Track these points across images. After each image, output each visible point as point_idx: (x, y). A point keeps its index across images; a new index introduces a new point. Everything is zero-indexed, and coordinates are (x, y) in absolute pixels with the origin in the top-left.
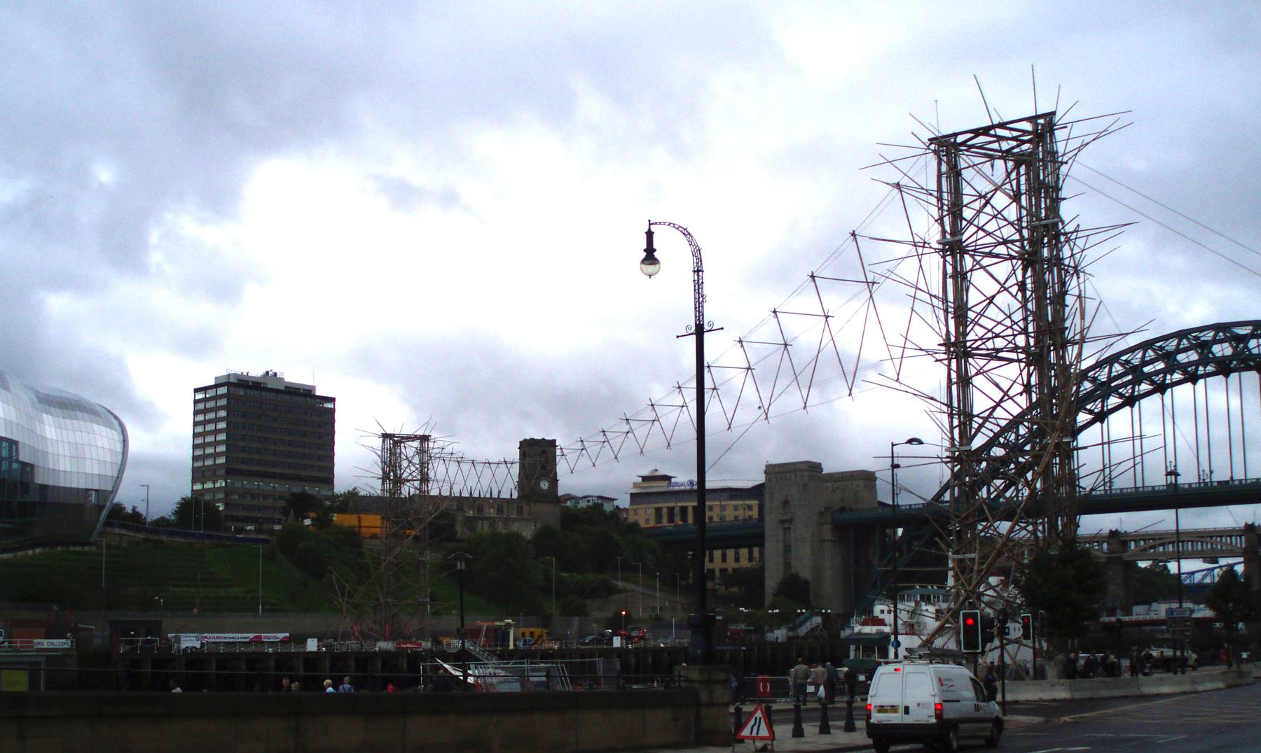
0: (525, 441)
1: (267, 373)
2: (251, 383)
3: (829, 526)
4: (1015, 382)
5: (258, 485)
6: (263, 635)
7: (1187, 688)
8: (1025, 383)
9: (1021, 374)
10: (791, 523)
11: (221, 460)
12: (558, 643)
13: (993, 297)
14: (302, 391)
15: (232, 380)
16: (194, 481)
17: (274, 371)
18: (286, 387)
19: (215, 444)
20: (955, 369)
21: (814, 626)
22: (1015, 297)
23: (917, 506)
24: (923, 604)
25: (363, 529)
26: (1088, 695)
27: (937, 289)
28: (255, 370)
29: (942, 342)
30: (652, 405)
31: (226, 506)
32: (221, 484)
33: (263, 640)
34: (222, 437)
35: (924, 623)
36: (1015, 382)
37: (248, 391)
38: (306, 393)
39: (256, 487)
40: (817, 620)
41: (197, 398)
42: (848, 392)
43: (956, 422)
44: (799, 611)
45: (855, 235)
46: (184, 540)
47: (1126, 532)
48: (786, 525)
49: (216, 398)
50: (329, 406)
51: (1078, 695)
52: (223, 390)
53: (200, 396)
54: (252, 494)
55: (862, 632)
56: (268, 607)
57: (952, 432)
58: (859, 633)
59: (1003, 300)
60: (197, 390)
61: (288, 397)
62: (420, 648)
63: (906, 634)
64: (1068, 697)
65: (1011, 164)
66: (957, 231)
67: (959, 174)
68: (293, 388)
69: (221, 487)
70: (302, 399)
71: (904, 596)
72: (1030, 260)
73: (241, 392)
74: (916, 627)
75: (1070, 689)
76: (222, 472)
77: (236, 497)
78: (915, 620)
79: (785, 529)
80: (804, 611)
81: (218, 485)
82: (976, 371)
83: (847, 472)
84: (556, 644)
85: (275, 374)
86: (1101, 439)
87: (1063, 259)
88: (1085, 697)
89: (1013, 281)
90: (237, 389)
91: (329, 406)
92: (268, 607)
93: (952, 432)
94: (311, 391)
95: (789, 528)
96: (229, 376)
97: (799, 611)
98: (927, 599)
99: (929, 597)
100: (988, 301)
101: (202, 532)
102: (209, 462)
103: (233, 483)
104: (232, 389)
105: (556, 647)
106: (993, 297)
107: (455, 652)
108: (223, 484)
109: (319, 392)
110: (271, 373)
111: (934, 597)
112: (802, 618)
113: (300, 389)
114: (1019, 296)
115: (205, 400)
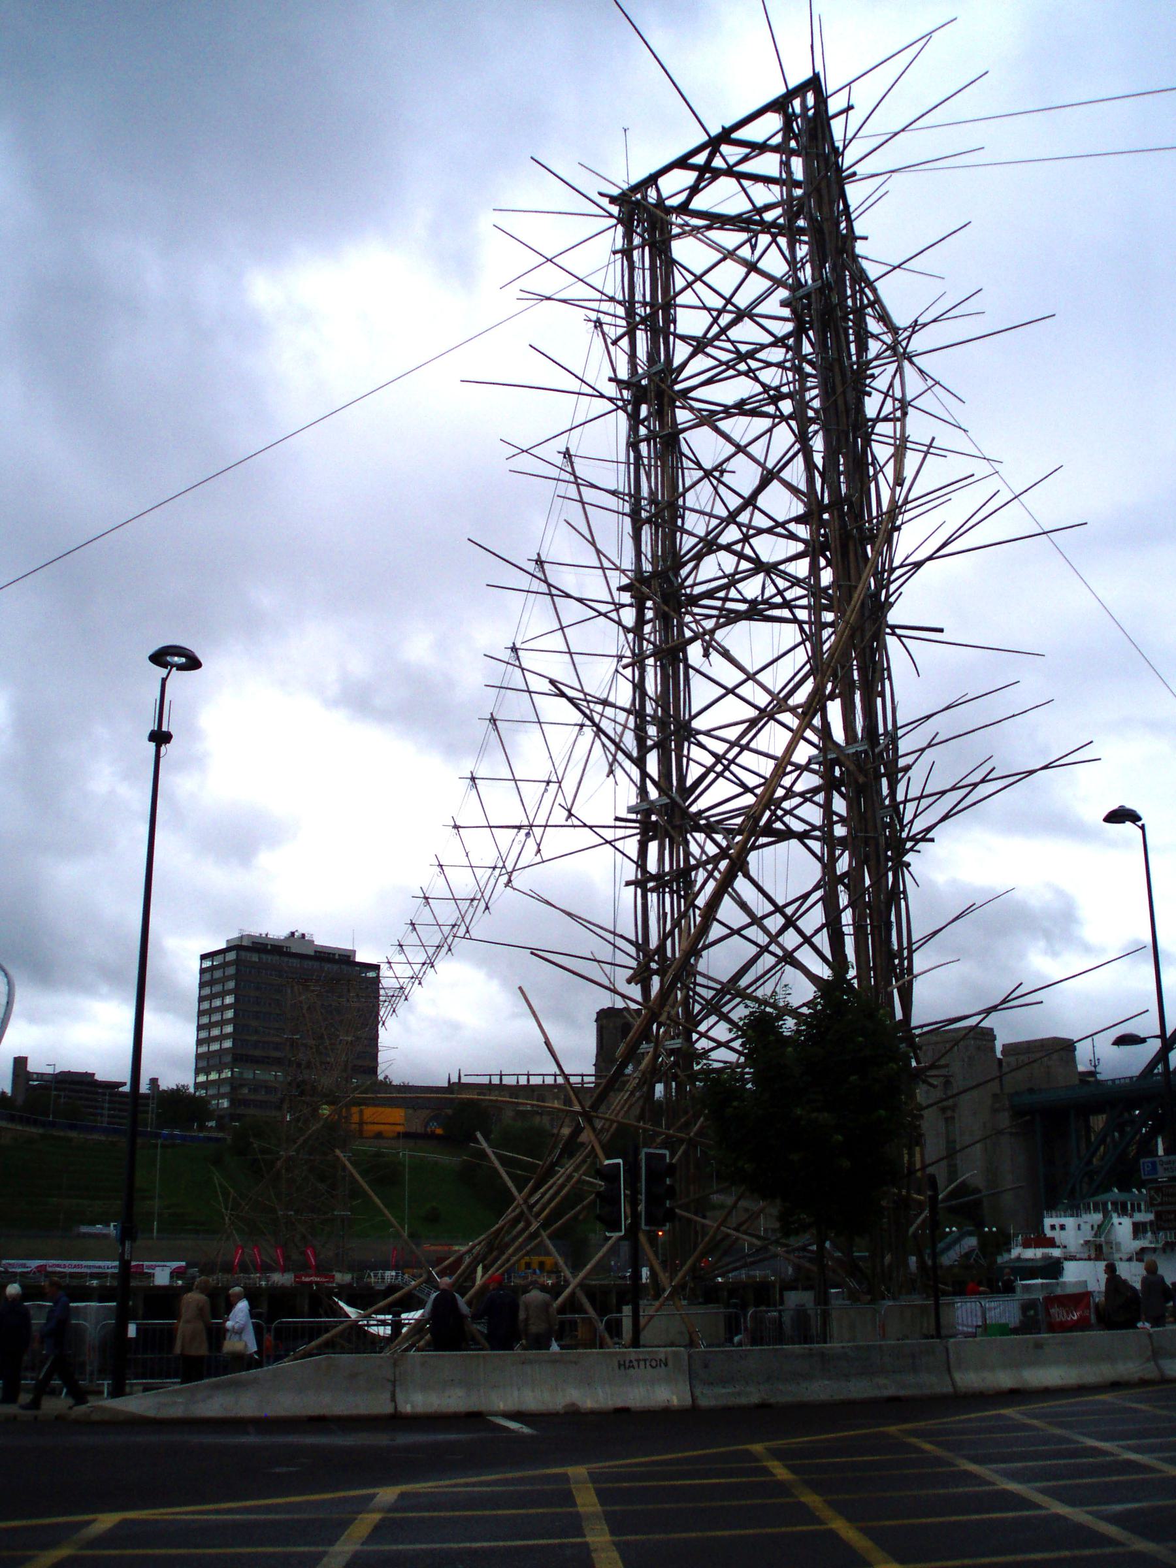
0: (602, 1010)
1: (293, 934)
2: (337, 957)
3: (1006, 1114)
5: (275, 1075)
6: (146, 1263)
7: (1129, 1369)
10: (953, 1111)
11: (228, 1044)
12: (554, 1276)
14: (337, 957)
15: (245, 943)
16: (198, 1071)
17: (301, 931)
18: (316, 952)
19: (222, 1023)
21: (963, 1252)
23: (1122, 1081)
24: (1115, 1215)
25: (366, 1127)
26: (753, 1395)
28: (277, 930)
30: (441, 866)
31: (232, 1102)
32: (227, 1074)
33: (146, 1271)
34: (230, 1014)
35: (1116, 1244)
37: (264, 957)
38: (345, 959)
39: (272, 1078)
40: (972, 1242)
41: (204, 966)
42: (606, 769)
44: (947, 1230)
45: (570, 456)
46: (103, 1138)
48: (949, 1113)
49: (224, 965)
50: (371, 974)
51: (710, 1398)
52: (231, 956)
53: (207, 964)
54: (266, 1087)
55: (1022, 1257)
56: (190, 1227)
58: (1019, 1259)
60: (203, 957)
61: (316, 964)
62: (332, 1282)
63: (1089, 1259)
64: (675, 1401)
68: (325, 953)
69: (226, 1078)
70: (336, 967)
71: (1105, 1204)
73: (255, 958)
74: (1105, 1249)
75: (692, 1377)
76: (228, 1059)
77: (246, 1091)
78: (1103, 1239)
79: (946, 1119)
80: (954, 1229)
81: (223, 1076)
83: (1036, 1041)
84: (549, 1278)
85: (303, 935)
86: (755, 670)
88: (743, 1401)
90: (249, 954)
91: (371, 974)
92: (190, 1227)
94: (349, 957)
95: (953, 1118)
96: (242, 938)
97: (947, 1230)
98: (1123, 1210)
99: (1124, 1206)
101: (51, 1119)
102: (215, 1047)
103: (241, 1073)
104: (243, 954)
105: (550, 1282)
107: (383, 1288)
108: (229, 1075)
109: (359, 958)
110: (296, 934)
111: (1132, 1205)
112: (948, 1240)
113: (334, 954)
115: (212, 969)
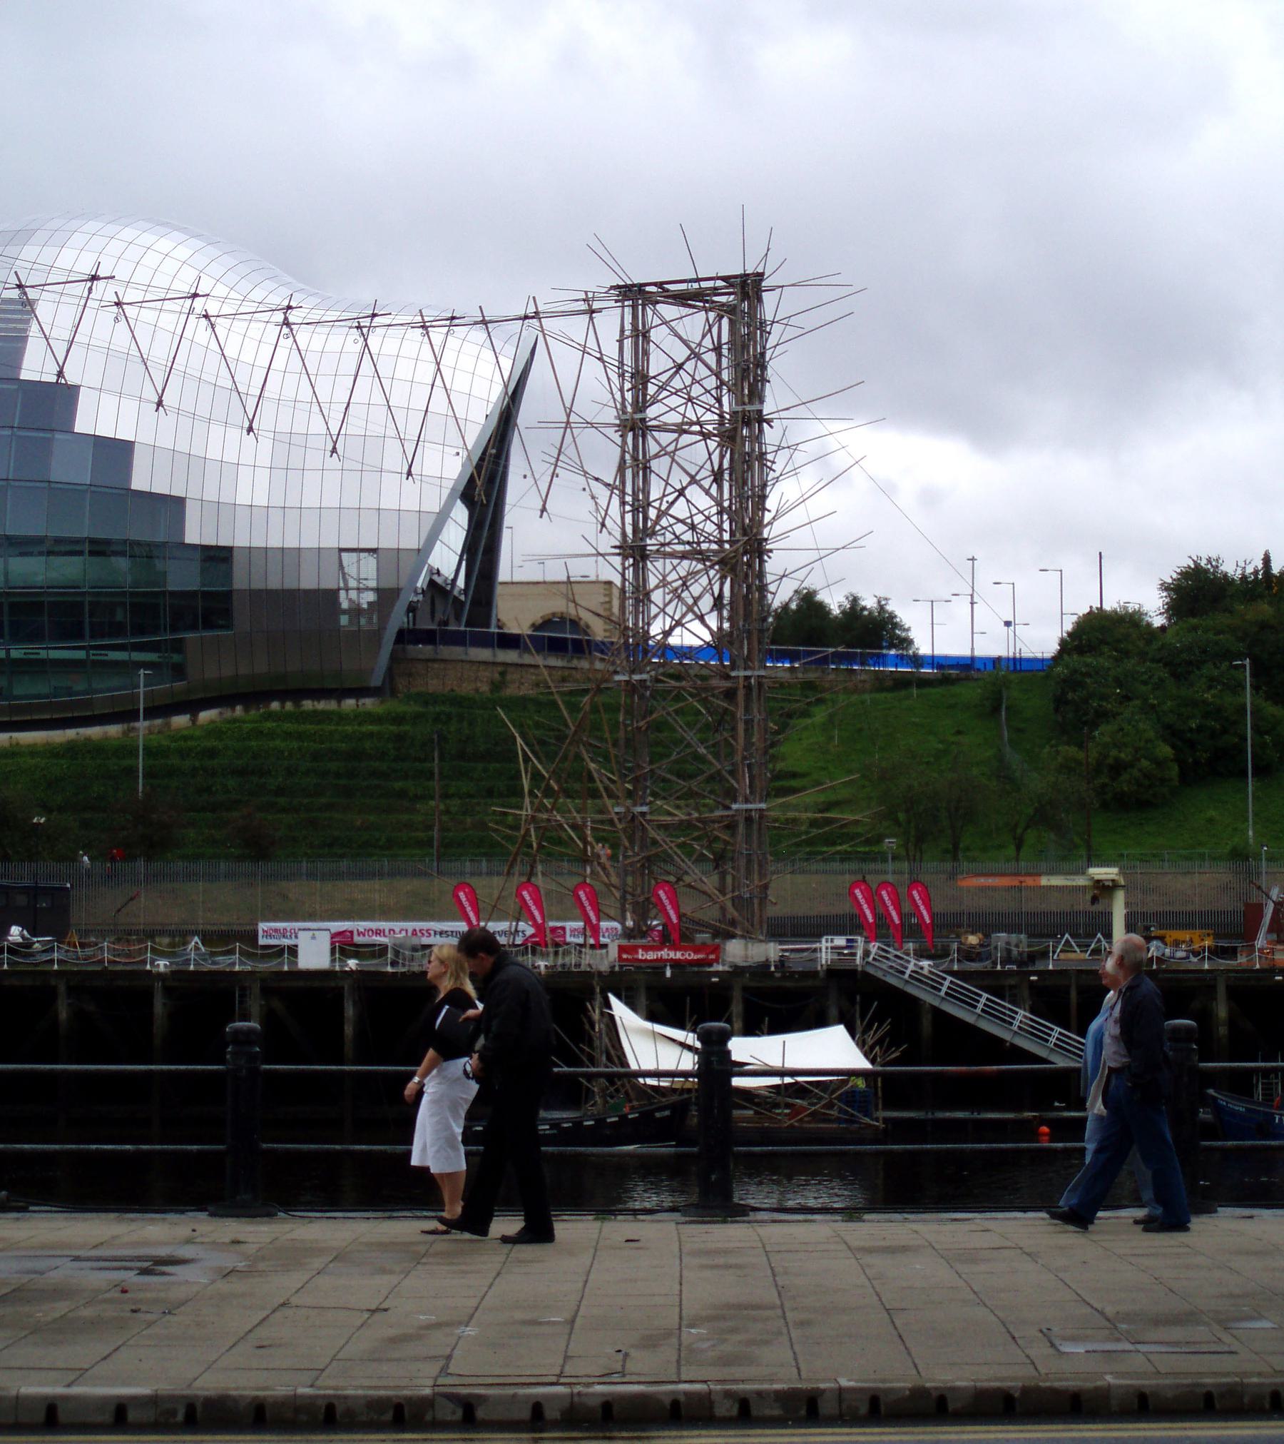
4: (702, 467)
8: (716, 468)
9: (710, 458)
13: (683, 364)
20: (630, 493)
22: (707, 492)
27: (611, 350)
29: (618, 544)
36: (702, 467)
43: (627, 385)
47: (809, 601)
57: (623, 518)
59: (694, 493)
65: (712, 315)
66: (641, 404)
67: (646, 336)
72: (728, 437)
82: (657, 581)
87: (766, 453)
89: (707, 343)
93: (623, 518)
100: (677, 494)
106: (683, 364)
114: (714, 490)
